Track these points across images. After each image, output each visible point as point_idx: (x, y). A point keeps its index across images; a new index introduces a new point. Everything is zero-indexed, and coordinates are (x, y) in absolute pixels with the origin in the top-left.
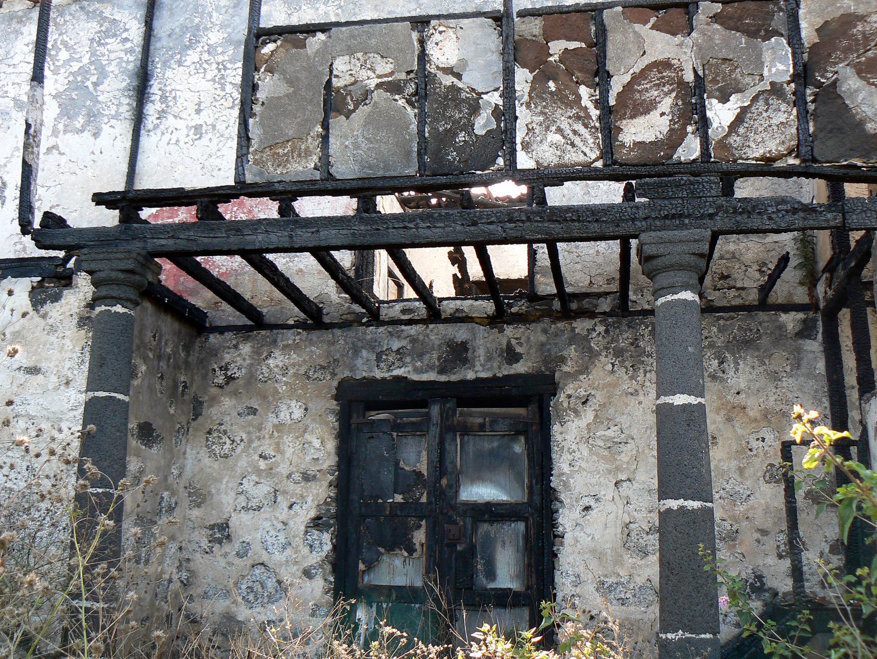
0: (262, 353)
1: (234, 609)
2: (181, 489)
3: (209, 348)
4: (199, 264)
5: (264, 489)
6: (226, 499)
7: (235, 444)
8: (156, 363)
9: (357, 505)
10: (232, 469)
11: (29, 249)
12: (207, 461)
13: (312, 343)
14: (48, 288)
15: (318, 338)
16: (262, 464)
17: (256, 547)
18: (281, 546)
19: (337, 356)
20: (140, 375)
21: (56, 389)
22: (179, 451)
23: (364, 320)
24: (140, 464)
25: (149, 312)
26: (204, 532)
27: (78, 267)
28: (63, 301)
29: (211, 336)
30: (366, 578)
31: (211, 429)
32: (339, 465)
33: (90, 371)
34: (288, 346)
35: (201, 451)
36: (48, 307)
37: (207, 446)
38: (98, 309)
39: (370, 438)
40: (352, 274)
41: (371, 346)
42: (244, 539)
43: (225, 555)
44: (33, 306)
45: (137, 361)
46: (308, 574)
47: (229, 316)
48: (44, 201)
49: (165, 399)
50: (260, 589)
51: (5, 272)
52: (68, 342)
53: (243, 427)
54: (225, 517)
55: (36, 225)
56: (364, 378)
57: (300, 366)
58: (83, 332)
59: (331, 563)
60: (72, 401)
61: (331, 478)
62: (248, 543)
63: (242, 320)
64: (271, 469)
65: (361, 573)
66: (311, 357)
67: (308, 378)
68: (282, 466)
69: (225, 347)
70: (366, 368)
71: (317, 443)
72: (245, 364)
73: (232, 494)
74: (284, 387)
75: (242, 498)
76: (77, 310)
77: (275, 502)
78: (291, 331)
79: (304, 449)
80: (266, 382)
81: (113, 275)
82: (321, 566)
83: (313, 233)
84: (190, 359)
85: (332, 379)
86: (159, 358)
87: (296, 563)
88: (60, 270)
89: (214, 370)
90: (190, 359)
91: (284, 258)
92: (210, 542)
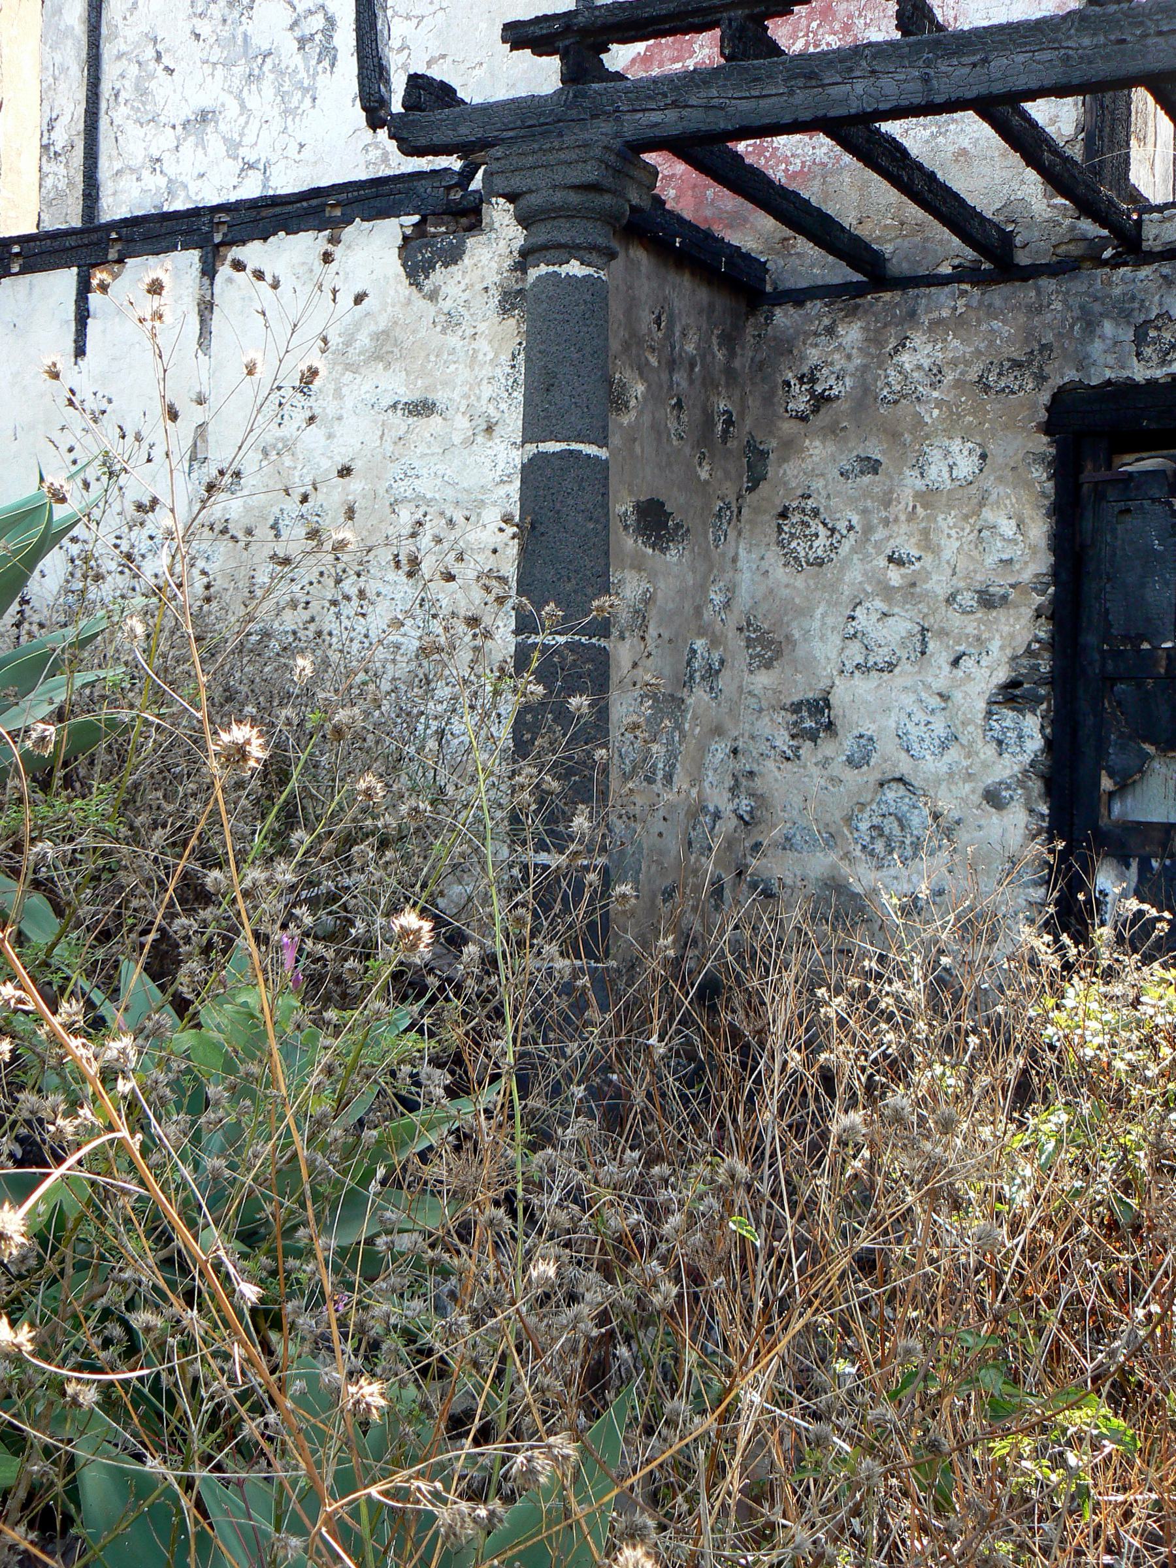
0: (886, 341)
1: (845, 868)
2: (731, 634)
3: (775, 338)
4: (738, 157)
5: (901, 626)
6: (823, 650)
7: (837, 535)
8: (665, 376)
9: (1097, 656)
10: (833, 587)
11: (376, 156)
12: (780, 573)
13: (992, 312)
14: (434, 236)
15: (1006, 299)
16: (895, 576)
17: (887, 746)
18: (937, 742)
19: (1049, 338)
20: (633, 403)
21: (470, 442)
22: (723, 555)
23: (1108, 254)
24: (645, 585)
25: (643, 269)
26: (783, 717)
27: (491, 190)
28: (467, 260)
29: (778, 312)
30: (1117, 808)
31: (786, 508)
32: (1056, 573)
33: (527, 403)
34: (939, 322)
35: (769, 555)
36: (439, 275)
37: (780, 544)
38: (533, 273)
39: (1121, 512)
40: (1076, 152)
41: (1122, 311)
42: (862, 731)
43: (825, 763)
44: (409, 276)
45: (624, 374)
46: (993, 798)
47: (812, 266)
48: (409, 53)
49: (687, 450)
50: (897, 831)
51: (348, 210)
52: (483, 345)
53: (852, 501)
54: (822, 685)
55: (397, 107)
56: (1109, 382)
57: (968, 363)
58: (512, 321)
59: (1042, 776)
60: (501, 466)
61: (1040, 599)
62: (871, 739)
63: (839, 272)
64: (914, 585)
65: (1104, 798)
66: (992, 343)
67: (987, 388)
68: (935, 577)
69: (807, 334)
70: (1113, 359)
71: (1008, 528)
72: (851, 367)
73: (836, 640)
74: (936, 412)
75: (855, 647)
76: (497, 279)
77: (923, 653)
78: (947, 289)
79: (980, 540)
80: (896, 402)
81: (558, 197)
82: (1021, 784)
83: (974, 65)
84: (737, 364)
85: (1038, 388)
86: (671, 365)
87: (970, 777)
88: (456, 195)
89: (788, 384)
90: (737, 364)
91: (925, 127)
92: (793, 737)
